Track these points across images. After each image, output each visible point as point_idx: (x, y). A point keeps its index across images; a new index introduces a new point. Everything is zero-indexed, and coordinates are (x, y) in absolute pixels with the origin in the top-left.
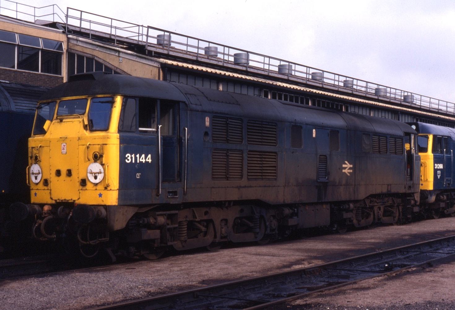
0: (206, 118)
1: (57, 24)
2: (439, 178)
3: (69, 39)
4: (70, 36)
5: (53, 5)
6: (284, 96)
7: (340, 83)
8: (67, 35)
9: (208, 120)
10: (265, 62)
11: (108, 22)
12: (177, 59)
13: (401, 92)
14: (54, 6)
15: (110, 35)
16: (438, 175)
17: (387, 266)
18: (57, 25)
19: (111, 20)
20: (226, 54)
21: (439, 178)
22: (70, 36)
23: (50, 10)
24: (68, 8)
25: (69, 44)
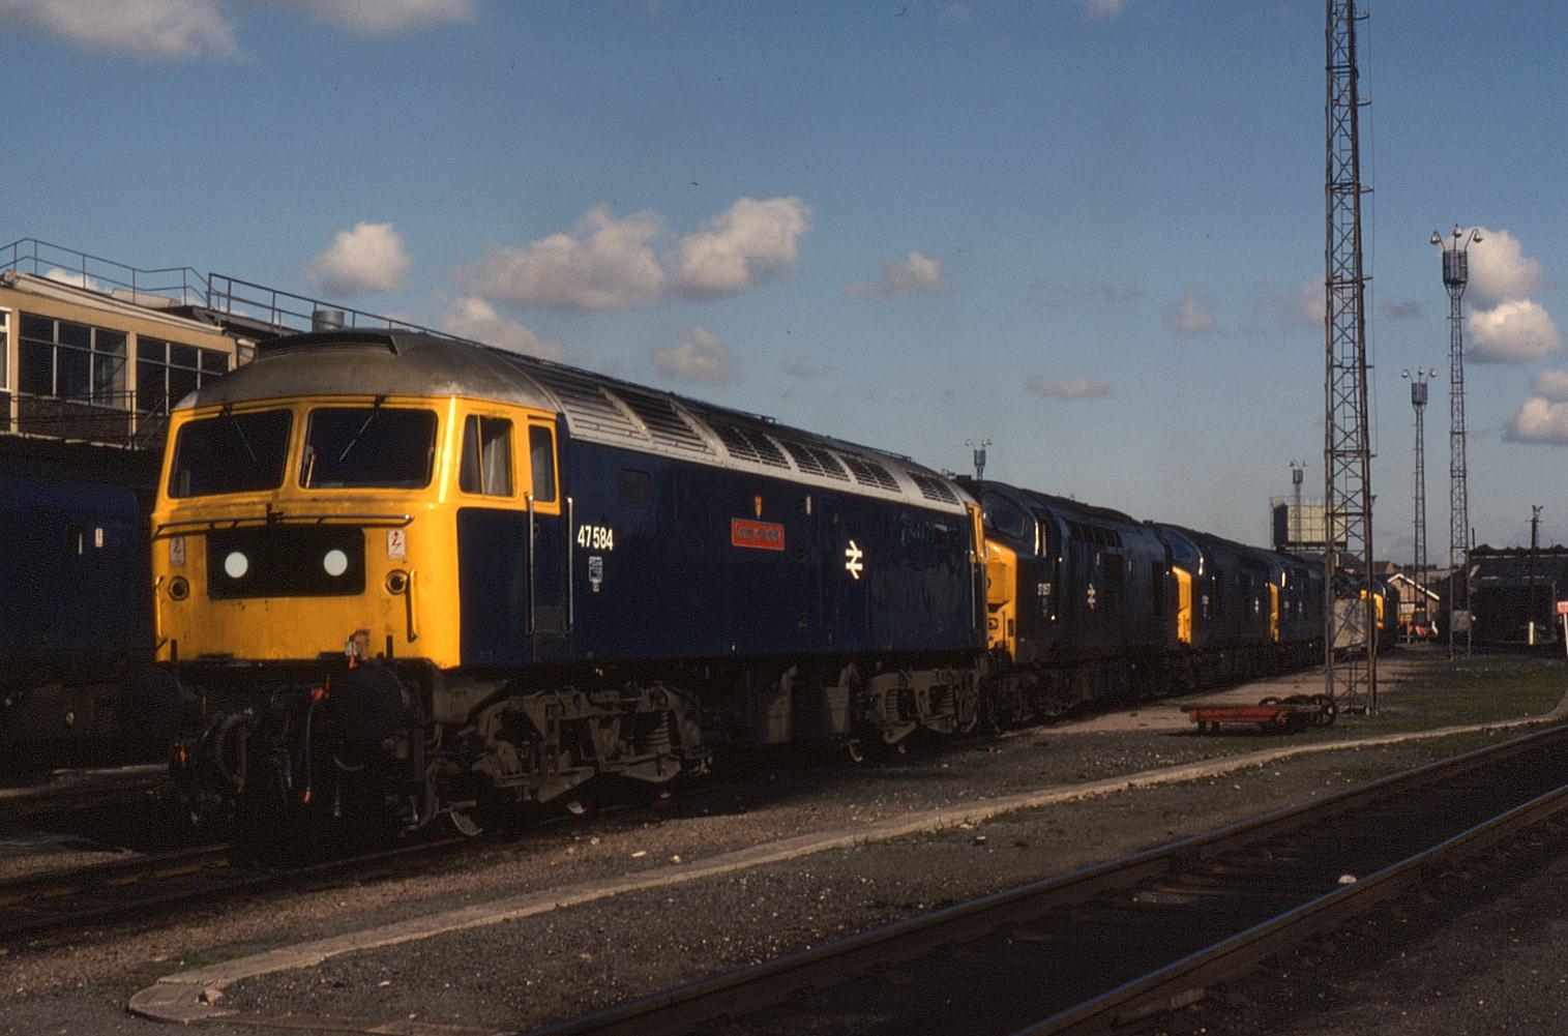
0: (97, 531)
1: (194, 309)
2: (596, 589)
3: (239, 346)
4: (242, 341)
5: (184, 269)
6: (202, 377)
7: (226, 292)
8: (236, 339)
9: (101, 535)
10: (232, 294)
11: (265, 298)
12: (1044, 527)
13: (1351, 675)
14: (187, 271)
15: (271, 325)
16: (594, 575)
17: (758, 560)
18: (195, 312)
19: (272, 294)
20: (224, 296)
21: (596, 589)
22: (242, 341)
23: (176, 279)
24: (211, 275)
25: (241, 357)
